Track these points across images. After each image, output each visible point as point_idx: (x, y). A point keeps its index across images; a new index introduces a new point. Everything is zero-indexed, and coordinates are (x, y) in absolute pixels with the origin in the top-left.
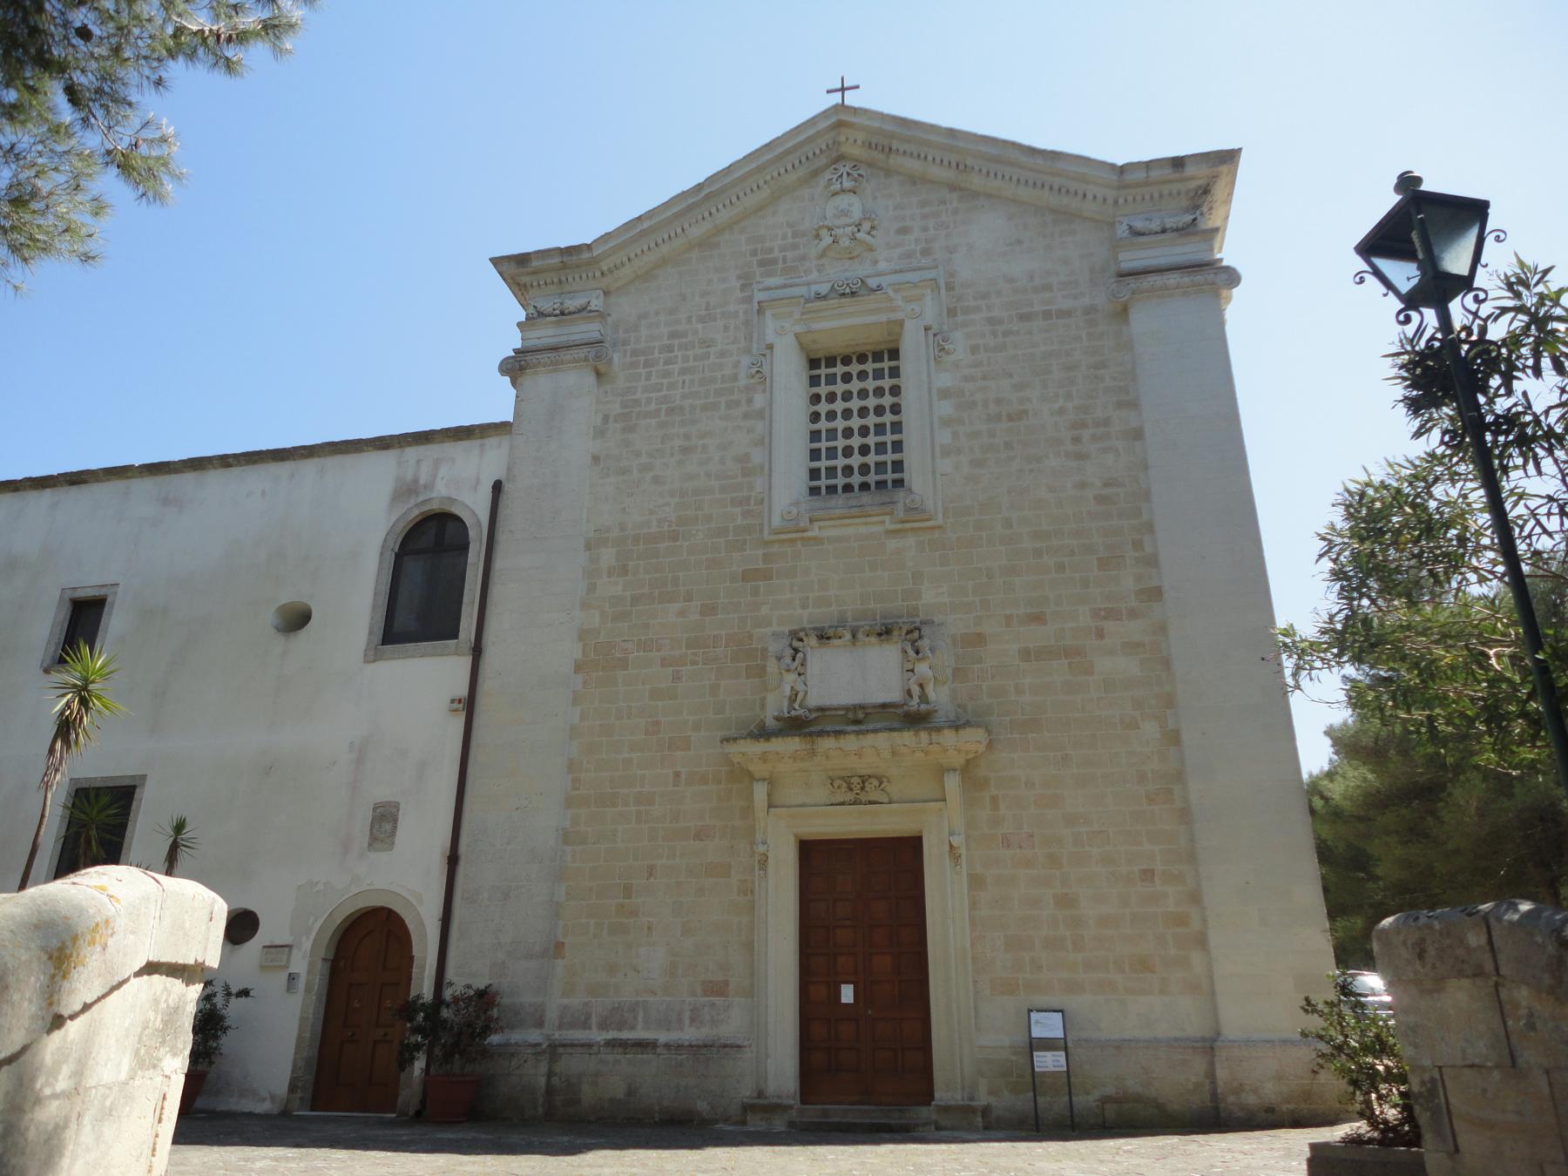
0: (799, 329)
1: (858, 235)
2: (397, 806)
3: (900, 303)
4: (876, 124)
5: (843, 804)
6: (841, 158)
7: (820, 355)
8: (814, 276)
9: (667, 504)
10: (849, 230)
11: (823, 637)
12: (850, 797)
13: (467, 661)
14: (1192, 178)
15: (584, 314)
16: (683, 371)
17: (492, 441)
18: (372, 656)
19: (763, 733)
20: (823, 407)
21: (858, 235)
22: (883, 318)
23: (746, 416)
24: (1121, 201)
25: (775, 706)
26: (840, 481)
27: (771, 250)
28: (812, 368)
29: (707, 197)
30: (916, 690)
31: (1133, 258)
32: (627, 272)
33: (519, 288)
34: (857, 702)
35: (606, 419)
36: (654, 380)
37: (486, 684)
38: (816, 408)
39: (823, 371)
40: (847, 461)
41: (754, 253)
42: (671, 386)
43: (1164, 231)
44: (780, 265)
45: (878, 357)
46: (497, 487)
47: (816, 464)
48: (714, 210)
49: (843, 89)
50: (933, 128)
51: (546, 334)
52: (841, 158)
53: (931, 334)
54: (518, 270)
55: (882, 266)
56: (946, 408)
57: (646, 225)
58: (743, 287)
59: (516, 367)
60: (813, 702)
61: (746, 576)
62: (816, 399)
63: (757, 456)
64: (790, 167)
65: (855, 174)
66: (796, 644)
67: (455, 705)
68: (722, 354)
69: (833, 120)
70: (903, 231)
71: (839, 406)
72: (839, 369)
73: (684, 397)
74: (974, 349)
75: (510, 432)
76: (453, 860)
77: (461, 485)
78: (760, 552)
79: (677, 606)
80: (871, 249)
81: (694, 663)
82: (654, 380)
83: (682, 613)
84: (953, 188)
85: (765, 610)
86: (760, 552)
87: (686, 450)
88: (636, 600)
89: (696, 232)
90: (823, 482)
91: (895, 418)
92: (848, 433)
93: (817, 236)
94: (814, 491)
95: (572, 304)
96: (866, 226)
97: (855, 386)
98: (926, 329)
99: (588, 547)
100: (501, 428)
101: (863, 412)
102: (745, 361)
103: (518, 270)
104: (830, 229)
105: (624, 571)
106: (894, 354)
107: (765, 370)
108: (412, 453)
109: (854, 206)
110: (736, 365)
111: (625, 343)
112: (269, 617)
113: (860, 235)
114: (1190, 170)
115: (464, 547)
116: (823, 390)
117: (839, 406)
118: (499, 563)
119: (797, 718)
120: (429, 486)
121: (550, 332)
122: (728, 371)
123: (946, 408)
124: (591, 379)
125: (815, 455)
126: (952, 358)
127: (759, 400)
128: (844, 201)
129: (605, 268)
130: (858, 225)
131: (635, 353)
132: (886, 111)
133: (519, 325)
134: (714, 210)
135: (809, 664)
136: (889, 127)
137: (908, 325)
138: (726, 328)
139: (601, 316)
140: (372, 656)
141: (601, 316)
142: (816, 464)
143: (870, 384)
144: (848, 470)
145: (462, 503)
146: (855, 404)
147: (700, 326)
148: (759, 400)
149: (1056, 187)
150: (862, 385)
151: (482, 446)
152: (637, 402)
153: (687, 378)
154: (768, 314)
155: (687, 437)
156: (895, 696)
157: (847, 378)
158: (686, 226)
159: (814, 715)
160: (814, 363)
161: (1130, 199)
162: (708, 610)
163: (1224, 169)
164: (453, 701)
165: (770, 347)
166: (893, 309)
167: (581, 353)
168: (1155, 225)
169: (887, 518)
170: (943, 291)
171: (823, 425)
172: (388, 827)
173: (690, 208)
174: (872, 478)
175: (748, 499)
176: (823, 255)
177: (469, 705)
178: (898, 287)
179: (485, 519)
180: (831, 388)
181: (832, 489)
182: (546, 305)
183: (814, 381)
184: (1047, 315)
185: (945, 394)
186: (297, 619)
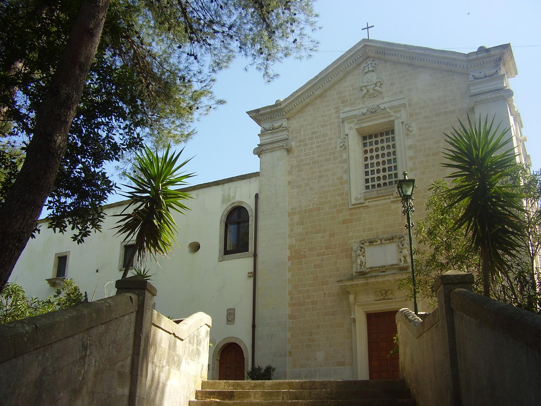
0: (357, 127)
1: (376, 88)
2: (234, 310)
3: (392, 113)
4: (378, 45)
5: (380, 300)
6: (368, 57)
7: (367, 134)
8: (361, 106)
9: (315, 198)
10: (372, 86)
11: (371, 242)
12: (382, 297)
13: (252, 259)
14: (494, 55)
15: (281, 129)
16: (318, 147)
17: (253, 179)
18: (221, 260)
19: (352, 278)
20: (369, 155)
21: (376, 88)
22: (387, 120)
23: (340, 162)
24: (469, 66)
25: (356, 268)
26: (376, 183)
27: (345, 97)
28: (369, 136)
29: (320, 80)
30: (403, 259)
31: (474, 90)
32: (294, 111)
33: (258, 122)
34: (383, 264)
35: (292, 167)
36: (307, 151)
37: (259, 267)
38: (366, 155)
39: (368, 141)
40: (379, 175)
41: (339, 98)
42: (313, 153)
43: (486, 77)
44: (349, 102)
45: (387, 133)
46: (257, 196)
47: (367, 177)
48: (323, 84)
49: (368, 28)
50: (399, 45)
51: (268, 138)
52: (368, 57)
53: (404, 124)
54: (257, 115)
55: (386, 99)
56: (410, 153)
57: (299, 93)
58: (336, 112)
59: (259, 151)
60: (368, 265)
61: (344, 222)
62: (366, 152)
63: (345, 177)
64: (349, 64)
65: (373, 63)
66: (362, 245)
67: (250, 275)
68: (330, 139)
69: (363, 45)
70: (392, 84)
71: (374, 154)
72: (374, 140)
73: (318, 157)
74: (420, 129)
75: (259, 175)
76: (254, 326)
77: (244, 195)
78: (348, 213)
79: (320, 235)
80: (381, 93)
81: (328, 254)
82: (307, 151)
83: (323, 237)
84: (410, 65)
85: (351, 234)
86: (348, 213)
87: (320, 177)
88: (307, 234)
89: (318, 93)
90: (370, 184)
91: (394, 157)
92: (378, 164)
93: (361, 90)
94: (367, 187)
95: (276, 125)
96: (379, 84)
97: (380, 145)
98: (402, 123)
99: (289, 215)
100: (256, 174)
101: (383, 155)
102: (339, 141)
103: (257, 115)
104: (366, 87)
105: (302, 223)
106: (393, 132)
107: (346, 144)
108: (227, 186)
109: (373, 77)
110: (336, 143)
111: (296, 138)
112: (187, 249)
113: (377, 88)
114: (493, 53)
115: (248, 221)
116: (368, 148)
117: (374, 154)
118: (260, 224)
119: (362, 272)
120: (234, 197)
121: (165, 361)
122: (333, 146)
123: (410, 153)
124: (285, 153)
125: (367, 173)
126: (413, 133)
127: (345, 156)
128: (369, 75)
129: (286, 111)
130: (376, 85)
131: (300, 141)
132: (381, 40)
133: (259, 135)
134: (323, 84)
135: (366, 252)
136: (382, 46)
137: (396, 122)
138: (331, 129)
139: (287, 129)
140: (221, 260)
141: (287, 129)
142: (367, 177)
143: (385, 144)
144: (379, 178)
145: (245, 203)
146: (380, 153)
147: (322, 129)
148: (345, 156)
149: (446, 63)
150: (382, 145)
151: (250, 181)
152: (302, 160)
153: (319, 149)
154: (346, 122)
155: (320, 172)
156: (395, 262)
157: (377, 142)
158: (314, 91)
159: (369, 270)
160: (364, 138)
161: (473, 65)
162: (332, 235)
163: (505, 51)
164: (249, 273)
165: (347, 135)
166: (390, 116)
167: (280, 144)
168: (482, 75)
169: (391, 197)
170: (408, 108)
171: (369, 162)
172: (232, 317)
173: (314, 85)
174: (387, 181)
175: (343, 193)
176: (364, 97)
177: (254, 275)
178: (391, 108)
179: (253, 207)
180: (371, 147)
181: (373, 186)
182: (267, 126)
183: (365, 145)
184: (446, 113)
185: (410, 147)
186: (195, 247)
